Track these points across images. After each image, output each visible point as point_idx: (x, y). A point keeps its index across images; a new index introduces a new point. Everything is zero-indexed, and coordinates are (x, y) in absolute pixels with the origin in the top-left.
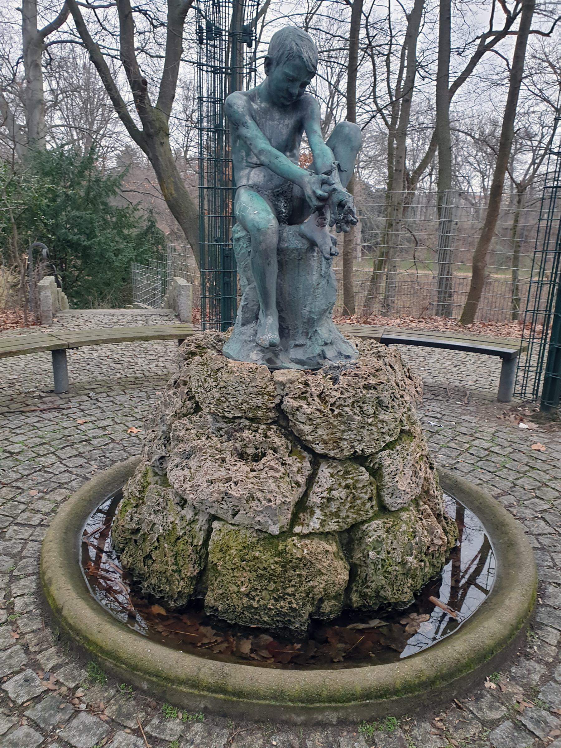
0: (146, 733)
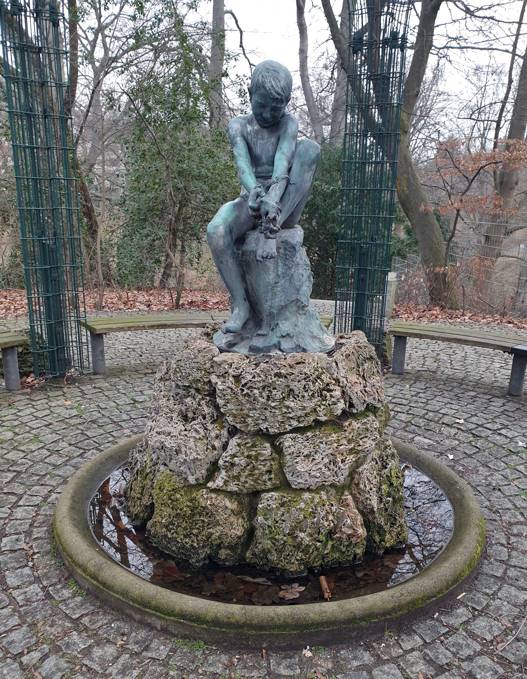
0: (48, 591)
